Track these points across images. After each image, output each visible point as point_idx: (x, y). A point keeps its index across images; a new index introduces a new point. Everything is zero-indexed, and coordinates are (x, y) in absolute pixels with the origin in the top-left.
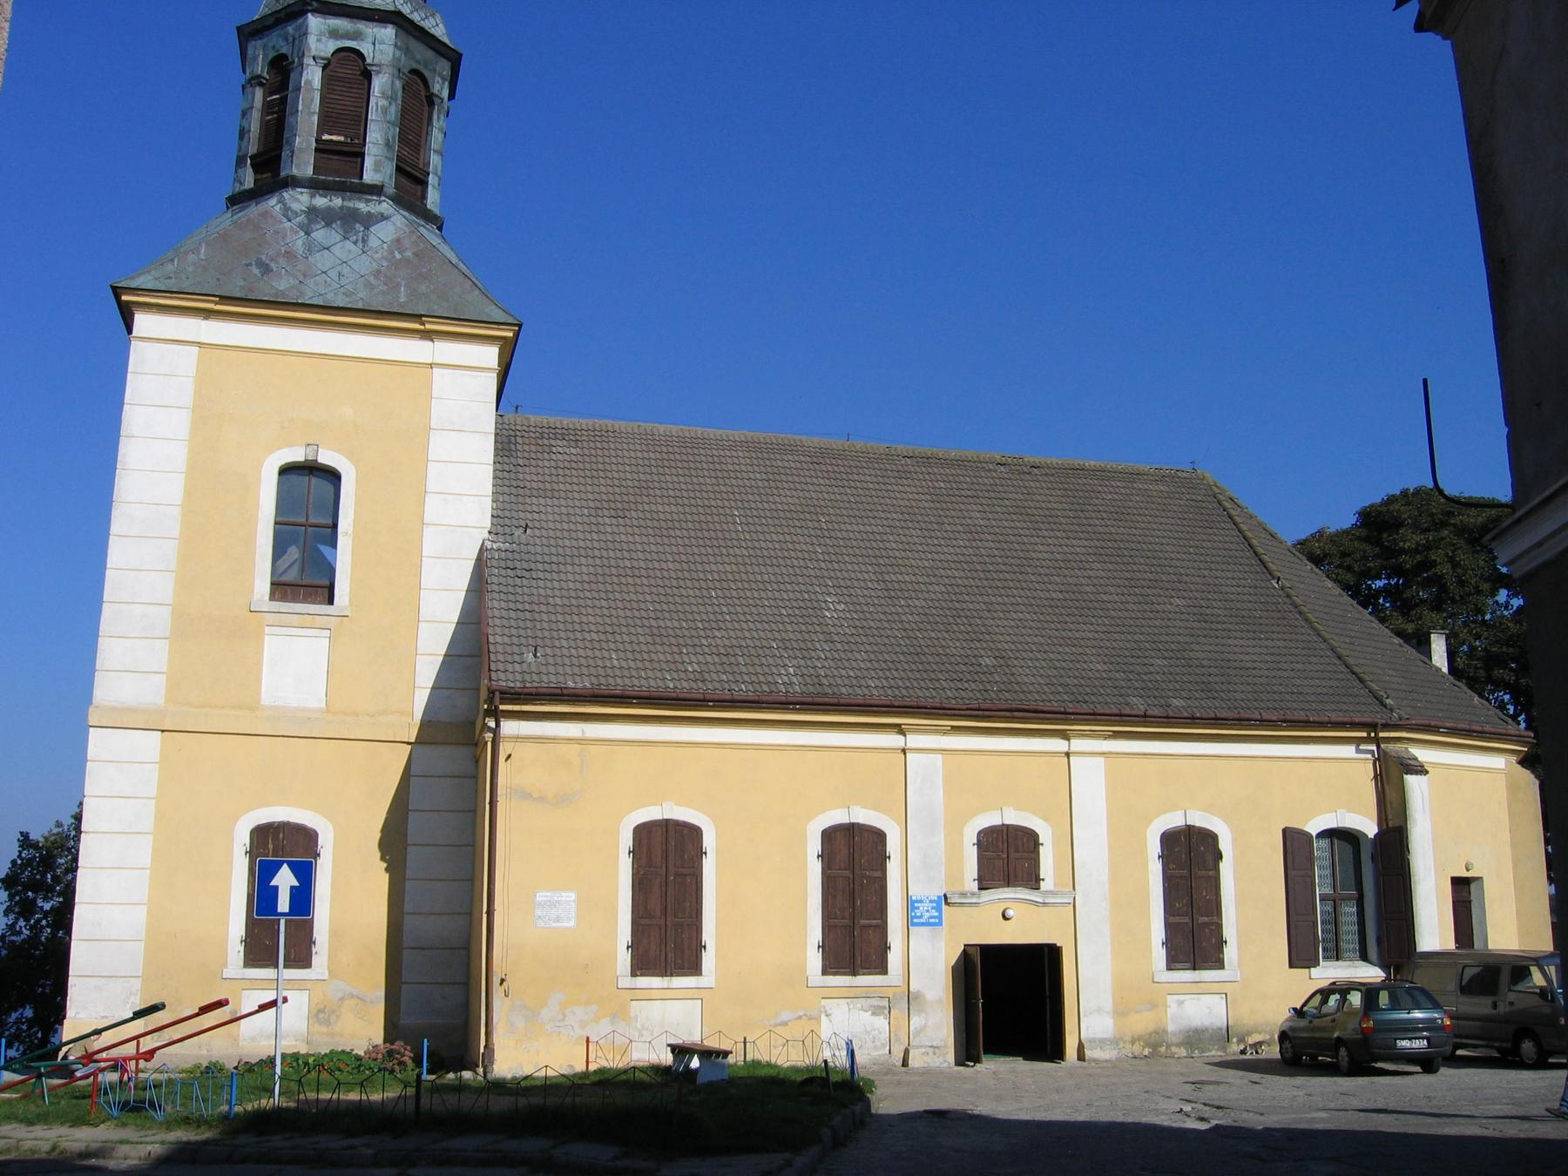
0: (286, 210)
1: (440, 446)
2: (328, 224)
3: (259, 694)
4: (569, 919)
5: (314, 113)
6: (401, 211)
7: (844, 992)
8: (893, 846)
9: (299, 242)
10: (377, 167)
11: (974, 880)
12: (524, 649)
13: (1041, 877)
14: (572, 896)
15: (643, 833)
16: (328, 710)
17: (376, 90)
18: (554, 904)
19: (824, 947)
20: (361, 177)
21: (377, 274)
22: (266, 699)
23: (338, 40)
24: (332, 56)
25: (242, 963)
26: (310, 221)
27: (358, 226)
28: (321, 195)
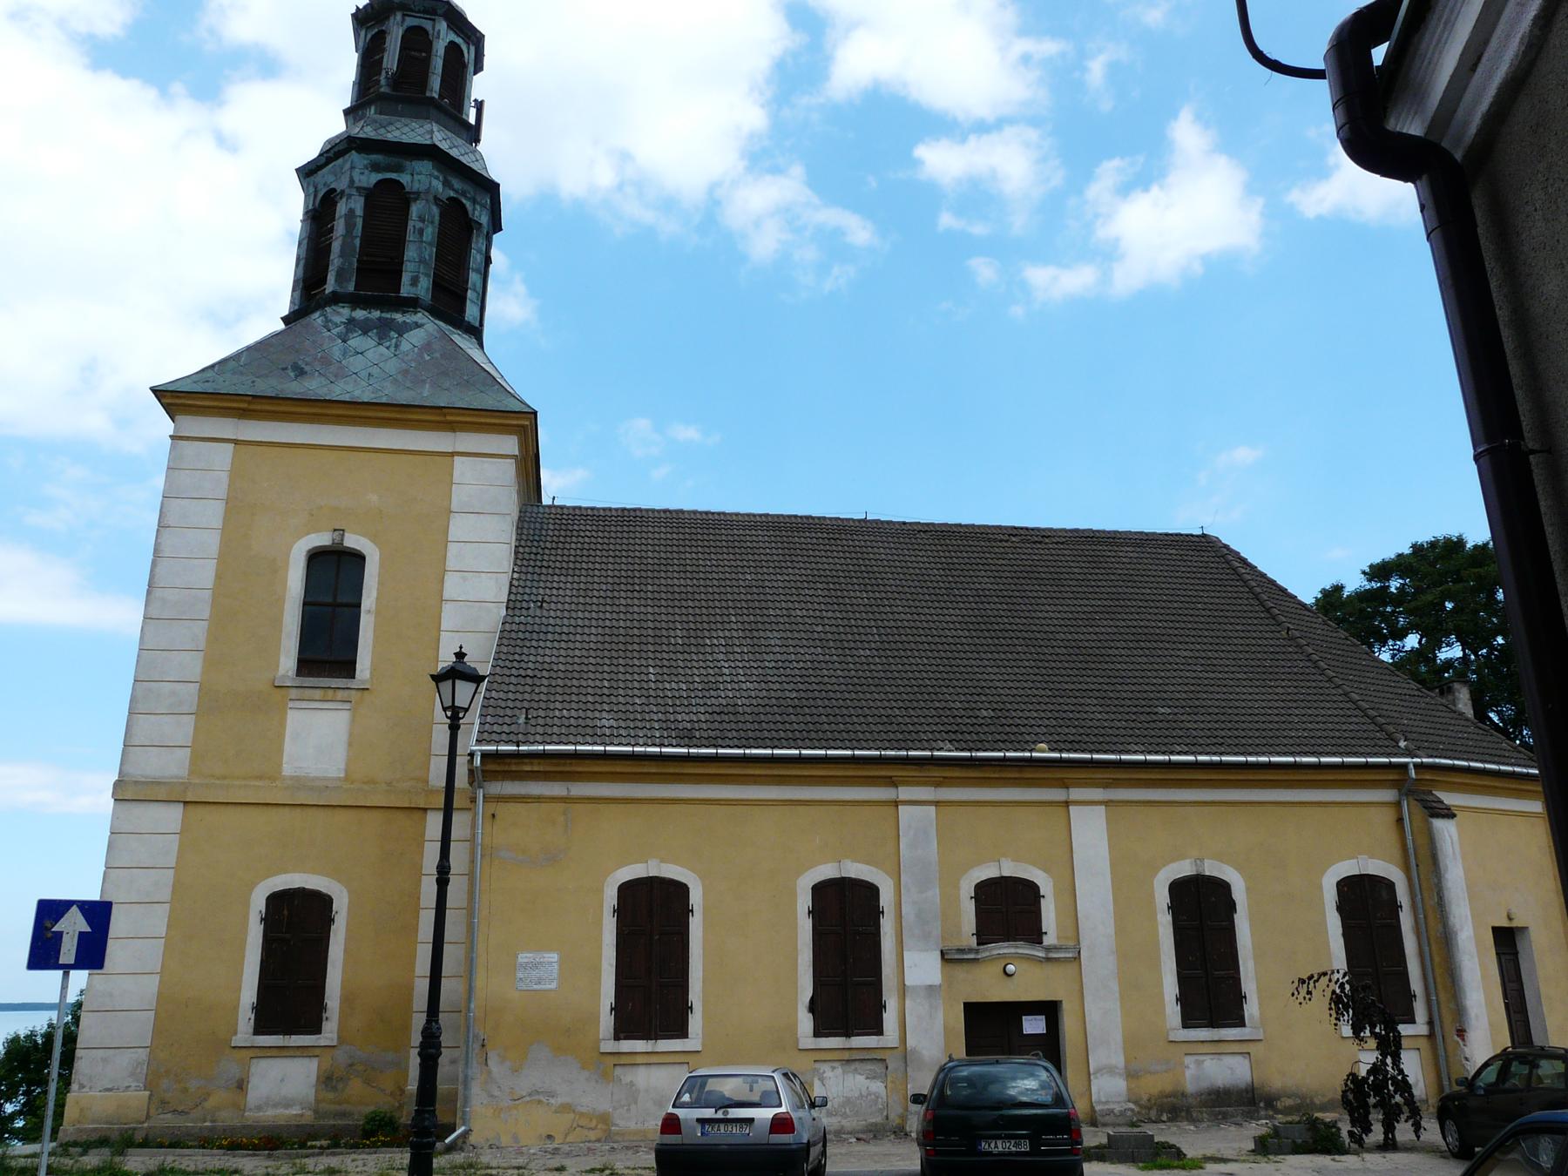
0: (327, 320)
1: (459, 528)
2: (365, 333)
3: (280, 765)
4: (552, 981)
5: (357, 237)
6: (437, 322)
7: (835, 1056)
8: (886, 899)
9: (336, 349)
10: (416, 280)
11: (973, 935)
12: (517, 712)
13: (1044, 931)
14: (554, 957)
15: (628, 890)
16: (346, 779)
17: (414, 215)
18: (535, 966)
19: (1182, 999)
20: (398, 290)
21: (405, 372)
22: (288, 770)
23: (379, 172)
24: (374, 186)
25: (251, 1030)
26: (348, 331)
27: (392, 333)
28: (361, 309)
